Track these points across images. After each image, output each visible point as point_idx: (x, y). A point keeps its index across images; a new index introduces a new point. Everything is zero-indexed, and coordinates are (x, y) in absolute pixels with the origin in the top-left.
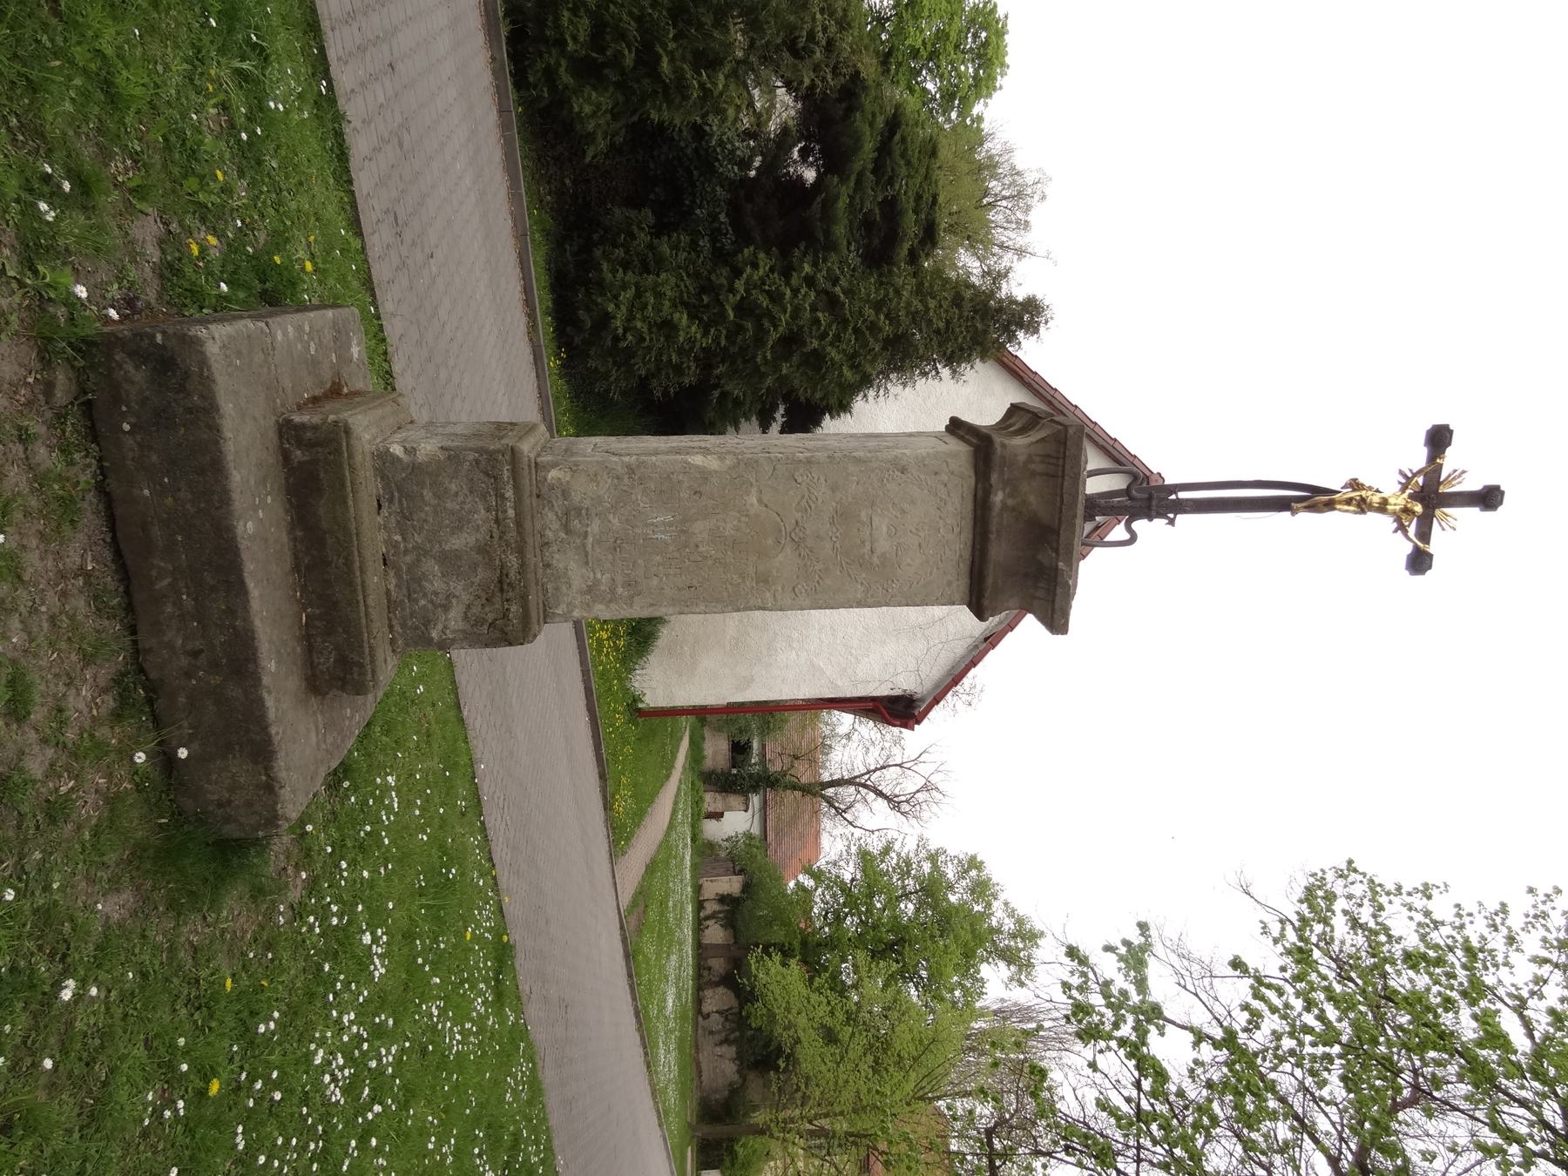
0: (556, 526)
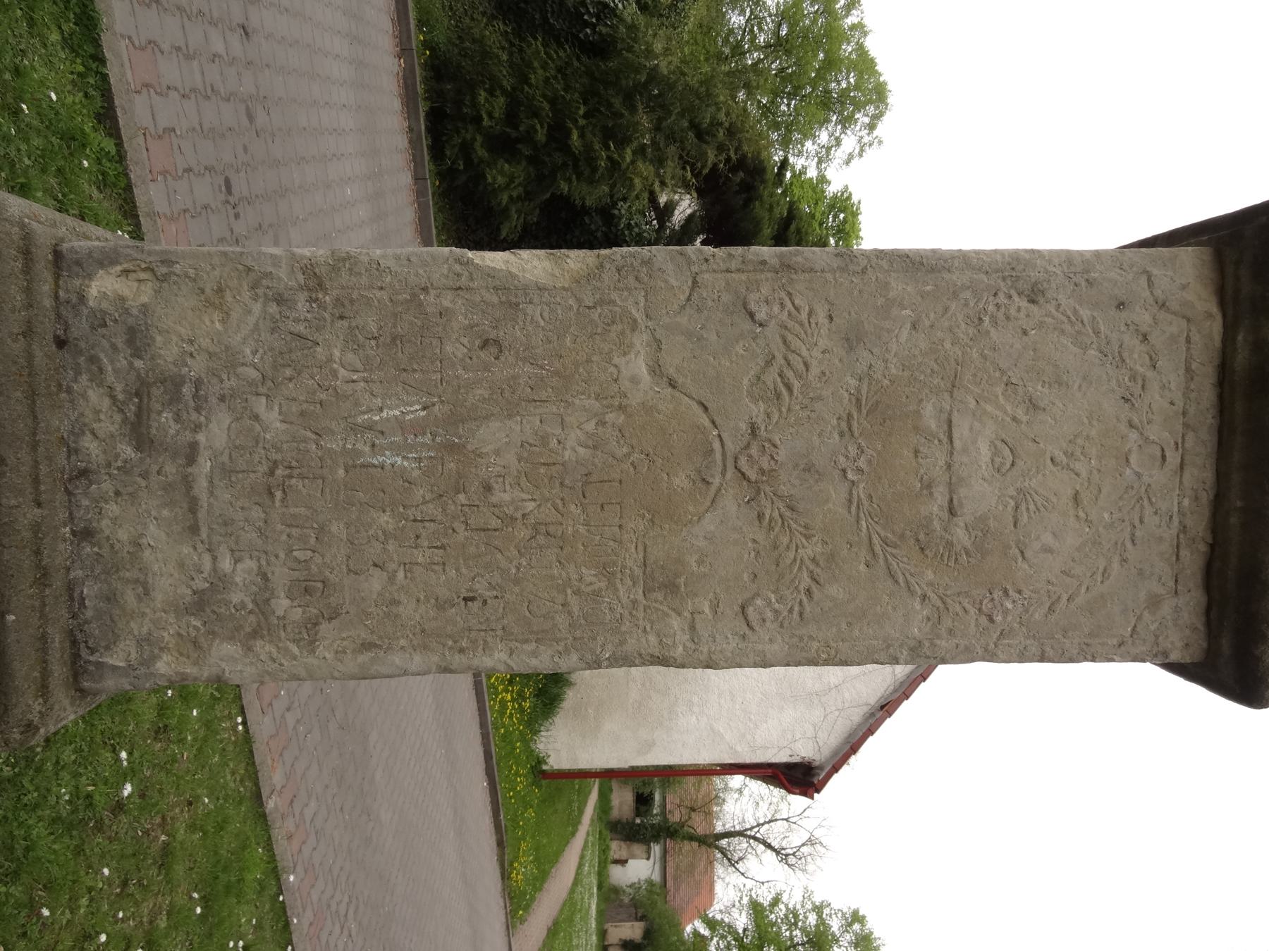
0: (109, 425)
